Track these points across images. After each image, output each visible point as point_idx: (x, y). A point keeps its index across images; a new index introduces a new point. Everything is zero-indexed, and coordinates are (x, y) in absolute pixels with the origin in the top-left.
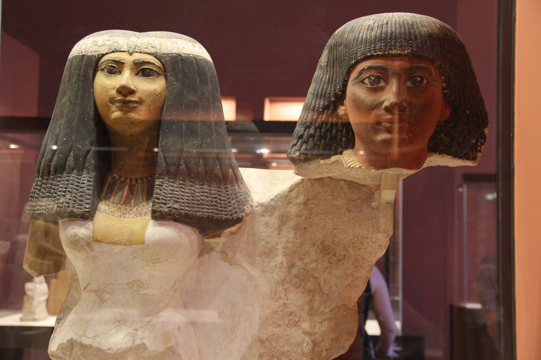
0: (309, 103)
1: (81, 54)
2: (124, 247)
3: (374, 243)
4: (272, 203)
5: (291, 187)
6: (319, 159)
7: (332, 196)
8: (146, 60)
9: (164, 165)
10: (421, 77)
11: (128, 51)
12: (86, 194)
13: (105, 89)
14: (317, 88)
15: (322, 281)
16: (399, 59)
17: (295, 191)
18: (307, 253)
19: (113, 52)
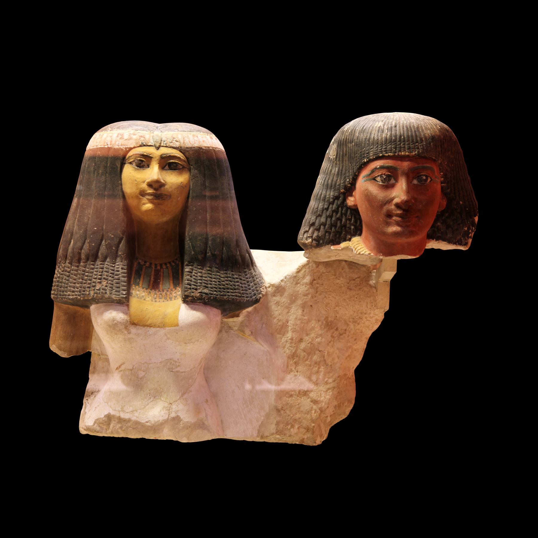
0: (320, 193)
1: (106, 147)
2: (158, 329)
3: (371, 318)
4: (283, 283)
5: (298, 269)
6: (330, 245)
7: (335, 275)
8: (172, 155)
9: (193, 253)
10: (427, 177)
11: (155, 146)
12: (122, 282)
13: (137, 183)
14: (327, 179)
15: (326, 354)
16: (407, 159)
17: (302, 272)
18: (313, 329)
19: (141, 146)
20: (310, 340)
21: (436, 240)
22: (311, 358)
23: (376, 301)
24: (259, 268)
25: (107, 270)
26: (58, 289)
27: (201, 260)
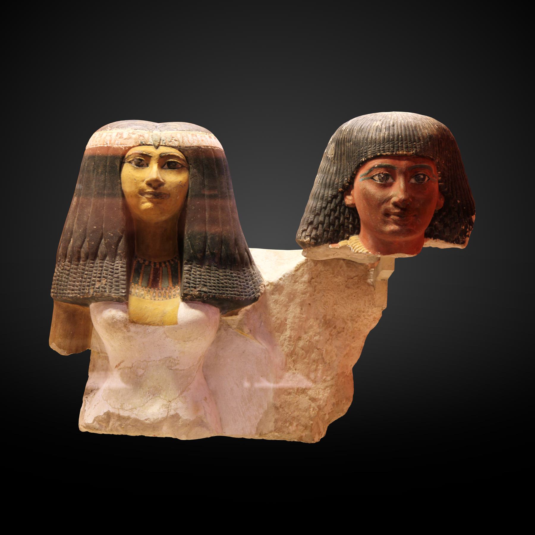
0: (318, 192)
1: (106, 146)
2: (157, 327)
3: (369, 316)
4: (281, 282)
5: (296, 267)
6: (328, 244)
7: (333, 274)
8: (171, 154)
9: (192, 251)
10: (424, 176)
11: (154, 145)
12: (121, 280)
13: (136, 182)
14: (325, 178)
15: (324, 352)
16: (405, 159)
17: (300, 270)
18: (311, 327)
19: (140, 145)
20: (308, 338)
21: (434, 239)
22: (309, 356)
23: (374, 299)
24: (257, 267)
25: (107, 268)
26: (57, 287)
27: (200, 259)
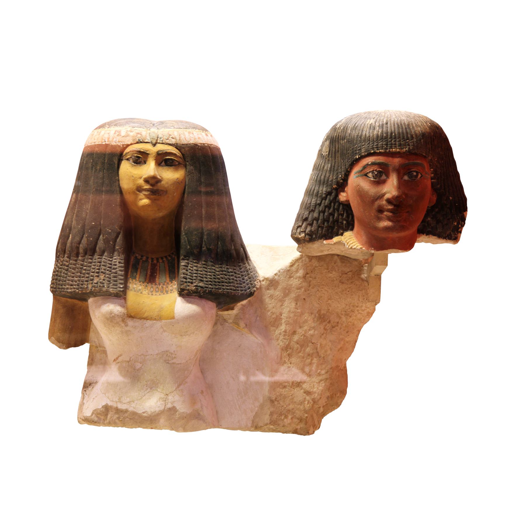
0: (313, 189)
1: (104, 143)
2: (154, 321)
3: (363, 310)
4: (276, 277)
5: (291, 263)
6: (322, 240)
7: (328, 269)
8: (168, 151)
9: (189, 247)
10: (417, 173)
11: (151, 143)
12: (119, 275)
13: (134, 179)
14: (320, 175)
15: (319, 346)
16: (398, 156)
17: (295, 266)
18: (306, 321)
19: (137, 143)
20: (303, 333)
21: (427, 235)
22: (304, 350)
23: (367, 294)
24: (253, 262)
25: (105, 264)
26: (56, 283)
27: (196, 254)
